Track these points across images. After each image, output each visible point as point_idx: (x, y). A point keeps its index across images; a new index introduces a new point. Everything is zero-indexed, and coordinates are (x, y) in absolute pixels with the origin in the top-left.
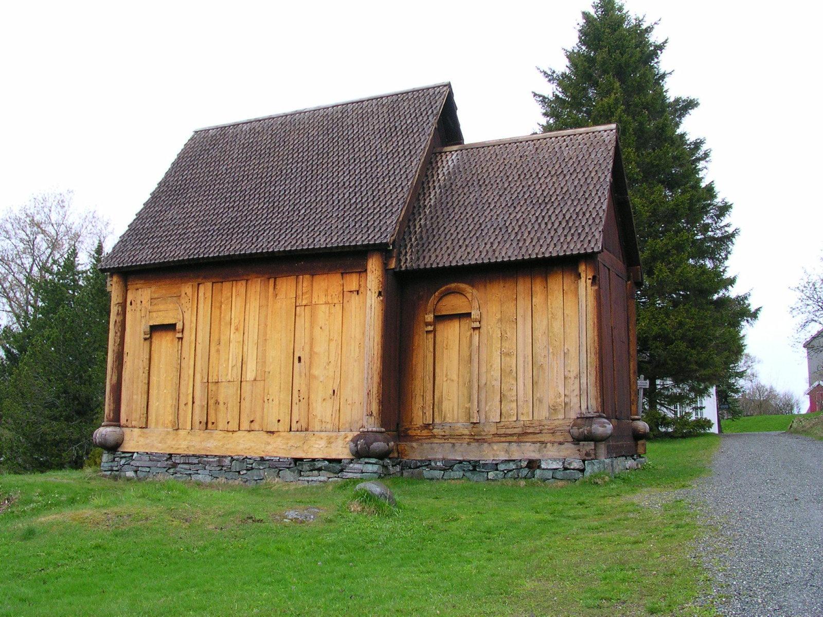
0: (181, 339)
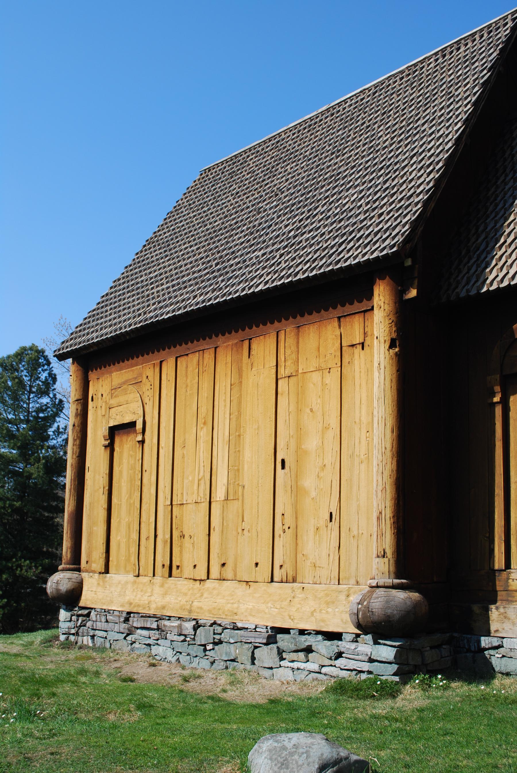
0: (142, 442)
